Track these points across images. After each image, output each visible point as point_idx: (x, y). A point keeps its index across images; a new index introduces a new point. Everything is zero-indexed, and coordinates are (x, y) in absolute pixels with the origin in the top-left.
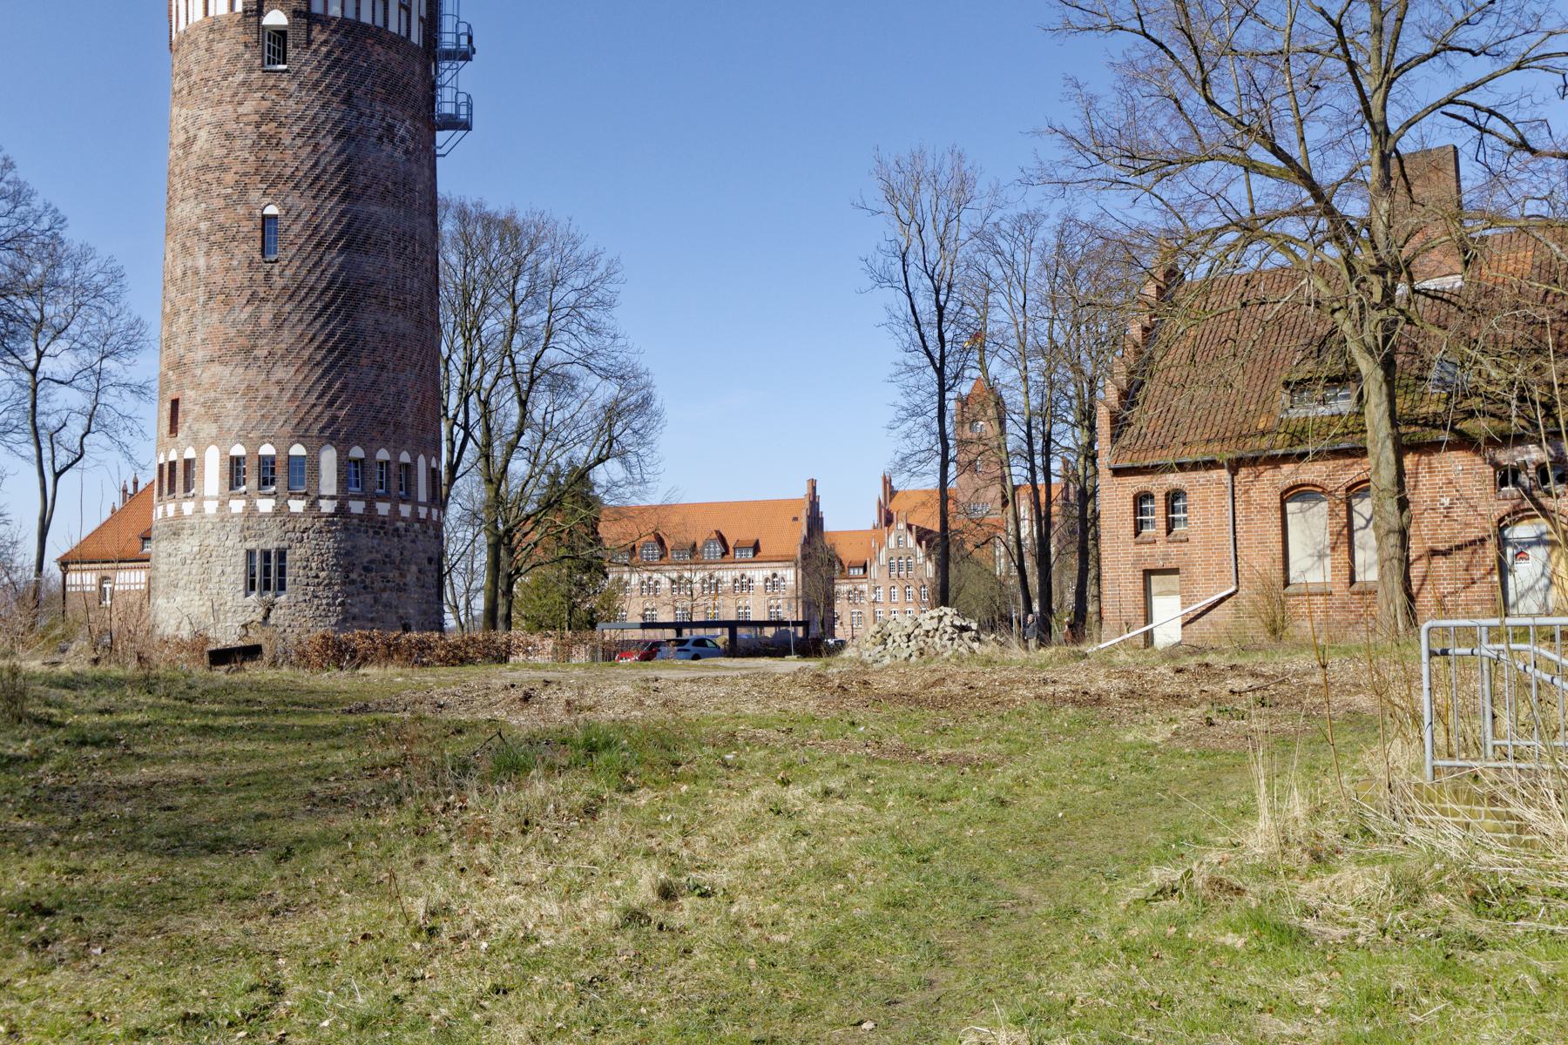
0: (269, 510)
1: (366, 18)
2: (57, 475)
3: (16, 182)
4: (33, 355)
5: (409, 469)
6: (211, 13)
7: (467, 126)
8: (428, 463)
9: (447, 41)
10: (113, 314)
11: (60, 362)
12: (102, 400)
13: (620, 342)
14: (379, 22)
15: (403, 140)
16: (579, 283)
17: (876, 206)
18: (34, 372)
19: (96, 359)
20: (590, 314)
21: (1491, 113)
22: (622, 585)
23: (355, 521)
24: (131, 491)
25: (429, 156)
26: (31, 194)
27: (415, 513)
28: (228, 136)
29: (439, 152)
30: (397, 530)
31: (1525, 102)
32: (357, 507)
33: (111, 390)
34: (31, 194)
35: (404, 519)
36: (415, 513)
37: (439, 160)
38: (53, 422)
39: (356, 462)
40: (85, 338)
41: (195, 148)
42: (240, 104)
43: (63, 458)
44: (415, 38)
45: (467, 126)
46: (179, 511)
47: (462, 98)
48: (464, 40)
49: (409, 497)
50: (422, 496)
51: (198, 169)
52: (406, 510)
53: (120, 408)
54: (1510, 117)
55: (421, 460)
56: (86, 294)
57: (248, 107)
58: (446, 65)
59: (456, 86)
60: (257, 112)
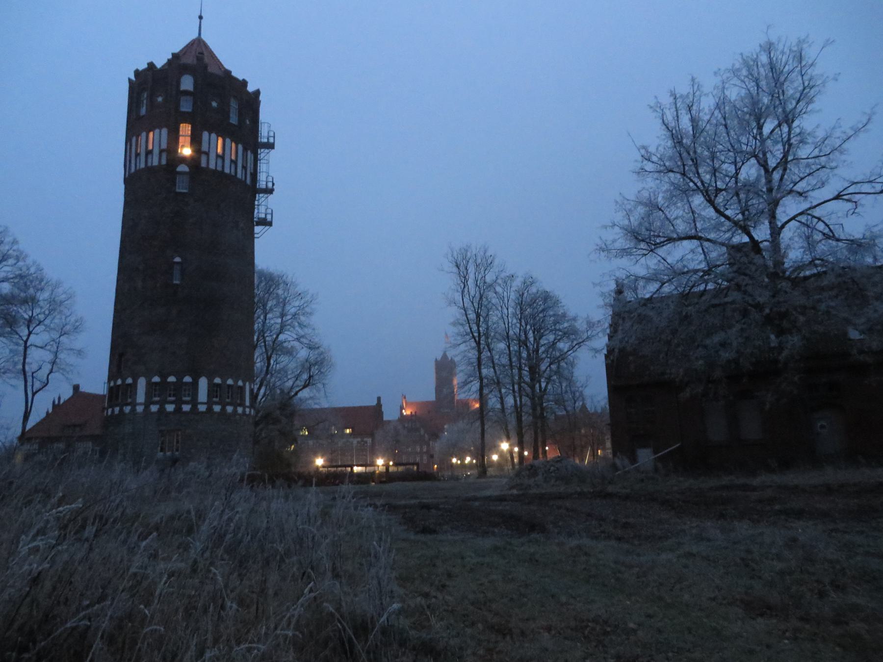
1: (227, 171)
2: (34, 394)
3: (18, 250)
4: (26, 332)
5: (242, 389)
6: (149, 164)
7: (270, 224)
9: (262, 184)
10: (68, 314)
11: (40, 337)
16: (297, 304)
17: (837, 226)
18: (26, 342)
20: (302, 318)
21: (819, 219)
24: (57, 402)
25: (251, 237)
26: (26, 256)
27: (244, 411)
29: (256, 236)
31: (833, 216)
32: (217, 408)
34: (26, 256)
35: (239, 415)
36: (244, 411)
37: (256, 240)
38: (35, 367)
43: (37, 385)
44: (248, 181)
45: (270, 224)
46: (121, 410)
48: (270, 185)
50: (248, 403)
52: (240, 410)
55: (247, 384)
56: (55, 305)
58: (261, 195)
59: (263, 206)
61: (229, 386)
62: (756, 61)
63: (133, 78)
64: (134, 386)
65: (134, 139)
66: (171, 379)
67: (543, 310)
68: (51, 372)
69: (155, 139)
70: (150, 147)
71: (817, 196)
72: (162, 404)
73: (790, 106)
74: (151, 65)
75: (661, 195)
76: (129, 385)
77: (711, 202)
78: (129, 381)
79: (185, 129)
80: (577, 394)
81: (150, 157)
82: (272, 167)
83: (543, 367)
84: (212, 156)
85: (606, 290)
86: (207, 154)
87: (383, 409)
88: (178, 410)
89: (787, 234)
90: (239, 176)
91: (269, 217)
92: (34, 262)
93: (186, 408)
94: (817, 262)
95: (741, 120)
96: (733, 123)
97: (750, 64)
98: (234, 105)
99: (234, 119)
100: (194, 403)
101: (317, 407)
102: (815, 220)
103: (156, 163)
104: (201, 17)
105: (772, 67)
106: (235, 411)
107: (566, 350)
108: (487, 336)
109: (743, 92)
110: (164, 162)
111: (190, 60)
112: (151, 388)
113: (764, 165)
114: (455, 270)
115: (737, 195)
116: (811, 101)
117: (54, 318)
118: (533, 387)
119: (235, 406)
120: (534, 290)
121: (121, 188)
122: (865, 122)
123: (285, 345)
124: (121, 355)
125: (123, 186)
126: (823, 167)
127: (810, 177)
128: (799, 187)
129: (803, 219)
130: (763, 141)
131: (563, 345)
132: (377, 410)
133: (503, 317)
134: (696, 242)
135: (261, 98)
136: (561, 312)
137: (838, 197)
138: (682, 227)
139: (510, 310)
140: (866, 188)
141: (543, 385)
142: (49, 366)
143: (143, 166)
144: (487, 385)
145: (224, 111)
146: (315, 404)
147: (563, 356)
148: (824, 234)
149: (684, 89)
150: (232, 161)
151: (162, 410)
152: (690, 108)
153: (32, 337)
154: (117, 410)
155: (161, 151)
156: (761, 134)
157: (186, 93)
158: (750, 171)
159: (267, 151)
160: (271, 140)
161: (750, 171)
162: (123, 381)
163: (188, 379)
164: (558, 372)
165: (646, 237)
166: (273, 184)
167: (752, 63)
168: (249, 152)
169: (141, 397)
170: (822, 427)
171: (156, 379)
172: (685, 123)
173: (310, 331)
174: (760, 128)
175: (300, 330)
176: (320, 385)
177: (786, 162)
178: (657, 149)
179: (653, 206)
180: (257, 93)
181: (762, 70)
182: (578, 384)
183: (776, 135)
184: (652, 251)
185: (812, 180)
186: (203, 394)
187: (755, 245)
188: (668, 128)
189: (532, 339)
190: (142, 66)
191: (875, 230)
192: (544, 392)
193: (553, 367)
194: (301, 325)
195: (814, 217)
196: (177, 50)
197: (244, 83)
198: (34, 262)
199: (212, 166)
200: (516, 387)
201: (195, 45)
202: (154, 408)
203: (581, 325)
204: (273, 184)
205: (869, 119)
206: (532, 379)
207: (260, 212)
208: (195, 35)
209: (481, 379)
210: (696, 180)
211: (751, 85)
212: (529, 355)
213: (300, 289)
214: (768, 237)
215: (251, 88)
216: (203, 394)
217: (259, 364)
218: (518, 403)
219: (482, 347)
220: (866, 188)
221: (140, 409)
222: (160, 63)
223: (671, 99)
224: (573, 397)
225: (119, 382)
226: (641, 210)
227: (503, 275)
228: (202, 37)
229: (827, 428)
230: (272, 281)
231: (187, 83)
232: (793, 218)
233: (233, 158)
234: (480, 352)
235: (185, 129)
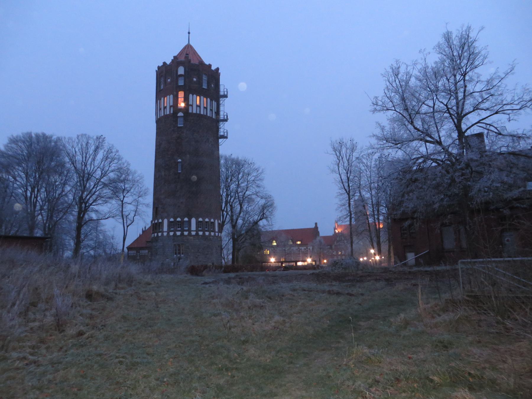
1: (202, 113)
2: (127, 226)
4: (122, 197)
5: (213, 223)
7: (226, 138)
9: (222, 117)
12: (138, 208)
13: (265, 189)
14: (205, 114)
16: (255, 174)
18: (122, 201)
20: (258, 182)
21: (490, 125)
31: (499, 122)
32: (201, 233)
40: (135, 193)
43: (129, 222)
44: (214, 117)
45: (226, 138)
48: (226, 117)
50: (217, 230)
52: (212, 234)
55: (216, 221)
58: (221, 123)
59: (224, 128)
61: (207, 222)
64: (162, 223)
66: (179, 219)
68: (135, 215)
69: (168, 100)
70: (165, 105)
72: (175, 231)
74: (165, 63)
76: (160, 223)
78: (160, 221)
79: (181, 94)
82: (227, 107)
84: (194, 106)
86: (192, 106)
87: (319, 230)
88: (182, 234)
90: (209, 115)
93: (186, 233)
98: (205, 78)
99: (205, 86)
100: (190, 231)
102: (488, 126)
103: (168, 113)
104: (189, 33)
106: (210, 234)
110: (172, 112)
111: (182, 59)
112: (170, 224)
114: (334, 153)
117: (135, 189)
119: (210, 231)
121: (154, 125)
124: (157, 208)
125: (155, 125)
129: (478, 124)
132: (315, 231)
143: (163, 115)
145: (200, 82)
150: (204, 108)
151: (175, 235)
153: (125, 198)
154: (156, 234)
155: (170, 107)
157: (181, 75)
162: (158, 221)
163: (186, 219)
168: (214, 102)
169: (165, 228)
171: (172, 220)
180: (218, 69)
186: (193, 227)
190: (161, 64)
194: (258, 186)
196: (176, 54)
197: (210, 66)
199: (194, 112)
202: (171, 234)
208: (187, 43)
213: (256, 166)
215: (213, 68)
216: (193, 227)
221: (165, 234)
222: (168, 62)
228: (191, 43)
230: (238, 165)
231: (181, 71)
233: (205, 106)
235: (181, 94)
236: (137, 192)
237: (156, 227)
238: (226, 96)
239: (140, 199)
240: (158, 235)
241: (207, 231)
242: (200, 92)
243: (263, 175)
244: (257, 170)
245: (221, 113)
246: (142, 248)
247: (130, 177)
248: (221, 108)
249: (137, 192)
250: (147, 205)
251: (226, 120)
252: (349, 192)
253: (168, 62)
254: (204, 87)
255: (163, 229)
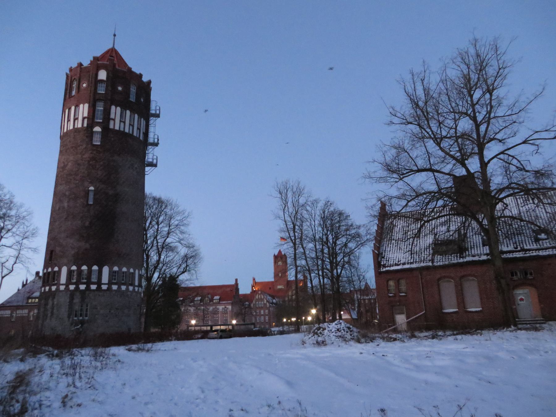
0: (95, 288)
1: (127, 130)
5: (133, 274)
6: (76, 127)
7: (156, 166)
8: (139, 272)
9: (151, 140)
12: (22, 252)
13: (191, 236)
14: (131, 132)
15: (136, 168)
16: (179, 218)
19: (21, 239)
20: (182, 228)
21: (513, 157)
22: (187, 311)
23: (114, 292)
25: (142, 175)
28: (79, 164)
29: (146, 173)
30: (128, 295)
31: (523, 155)
33: (25, 250)
35: (130, 291)
36: (134, 289)
39: (115, 272)
40: (18, 233)
41: (67, 168)
42: (84, 155)
44: (141, 138)
45: (156, 166)
46: (50, 289)
47: (155, 157)
48: (156, 141)
49: (132, 284)
50: (137, 284)
51: (67, 175)
52: (131, 288)
53: (27, 255)
54: (518, 159)
56: (19, 219)
57: (86, 156)
58: (150, 147)
59: (151, 154)
60: (89, 157)
61: (123, 272)
62: (467, 53)
63: (68, 72)
64: (59, 272)
65: (67, 111)
67: (339, 222)
68: (15, 263)
71: (511, 142)
72: (77, 284)
73: (489, 82)
75: (407, 141)
76: (55, 272)
77: (439, 144)
78: (56, 269)
80: (362, 277)
81: (76, 121)
82: (158, 129)
83: (339, 259)
85: (370, 204)
86: (114, 120)
87: (239, 287)
88: (88, 288)
89: (490, 168)
90: (135, 134)
91: (155, 161)
92: (9, 192)
94: (513, 185)
95: (460, 92)
96: (454, 94)
97: (463, 57)
98: (133, 90)
99: (133, 98)
101: (192, 285)
103: (80, 126)
104: (115, 35)
105: (478, 56)
106: (127, 289)
107: (353, 248)
108: (301, 238)
109: (459, 74)
110: (85, 125)
113: (474, 119)
114: (279, 196)
115: (457, 141)
116: (505, 77)
118: (332, 272)
120: (332, 209)
122: (541, 91)
123: (171, 245)
126: (515, 122)
127: (506, 129)
128: (499, 136)
129: (501, 156)
130: (473, 105)
131: (352, 245)
133: (313, 227)
134: (431, 174)
135: (151, 85)
136: (350, 223)
137: (524, 142)
138: (421, 163)
139: (317, 222)
140: (544, 135)
141: (339, 271)
142: (14, 259)
143: (71, 127)
144: (300, 272)
145: (127, 92)
146: (191, 283)
147: (352, 252)
148: (517, 167)
149: (418, 69)
152: (422, 81)
154: (47, 288)
155: (84, 118)
156: (472, 100)
157: (102, 81)
158: (465, 125)
159: (154, 119)
160: (158, 112)
161: (465, 125)
164: (349, 262)
165: (396, 170)
166: (158, 140)
167: (464, 54)
168: (142, 119)
169: (63, 279)
170: (522, 300)
172: (420, 93)
173: (187, 236)
174: (471, 96)
175: (180, 235)
176: (193, 272)
177: (489, 118)
178: (401, 108)
179: (400, 149)
180: (149, 82)
181: (471, 58)
182: (362, 271)
183: (482, 101)
184: (401, 179)
185: (508, 131)
186: (105, 278)
187: (470, 175)
188: (408, 95)
189: (331, 241)
190: (74, 65)
191: (551, 162)
192: (339, 276)
193: (346, 259)
194: (182, 233)
195: (509, 155)
196: (98, 54)
197: (140, 76)
198: (9, 192)
199: (117, 128)
200: (321, 273)
201: (110, 52)
203: (362, 231)
204: (158, 140)
205: (544, 89)
206: (331, 267)
207: (149, 158)
208: (111, 46)
209: (297, 267)
210: (428, 130)
211: (464, 67)
212: (329, 251)
213: (181, 209)
214: (479, 169)
216: (105, 278)
217: (154, 257)
218: (322, 282)
219: (297, 246)
220: (544, 135)
221: (62, 288)
223: (410, 76)
224: (359, 279)
225: (50, 270)
226: (394, 151)
227: (311, 199)
229: (525, 299)
231: (103, 75)
232: (495, 156)
234: (295, 250)
236: (21, 232)
237: (48, 278)
238: (158, 116)
239: (25, 241)
240: (50, 289)
241: (124, 284)
242: (125, 105)
243: (188, 219)
244: (183, 212)
245: (151, 135)
246: (18, 307)
247: (13, 213)
248: (151, 129)
249: (21, 232)
250: (35, 250)
251: (156, 145)
252: (295, 240)
253: (86, 63)
254: (131, 99)
255: (59, 280)
